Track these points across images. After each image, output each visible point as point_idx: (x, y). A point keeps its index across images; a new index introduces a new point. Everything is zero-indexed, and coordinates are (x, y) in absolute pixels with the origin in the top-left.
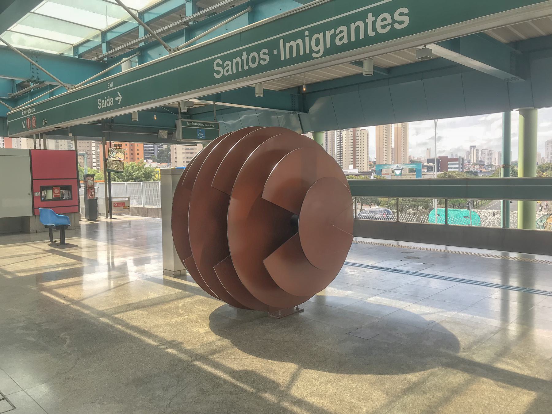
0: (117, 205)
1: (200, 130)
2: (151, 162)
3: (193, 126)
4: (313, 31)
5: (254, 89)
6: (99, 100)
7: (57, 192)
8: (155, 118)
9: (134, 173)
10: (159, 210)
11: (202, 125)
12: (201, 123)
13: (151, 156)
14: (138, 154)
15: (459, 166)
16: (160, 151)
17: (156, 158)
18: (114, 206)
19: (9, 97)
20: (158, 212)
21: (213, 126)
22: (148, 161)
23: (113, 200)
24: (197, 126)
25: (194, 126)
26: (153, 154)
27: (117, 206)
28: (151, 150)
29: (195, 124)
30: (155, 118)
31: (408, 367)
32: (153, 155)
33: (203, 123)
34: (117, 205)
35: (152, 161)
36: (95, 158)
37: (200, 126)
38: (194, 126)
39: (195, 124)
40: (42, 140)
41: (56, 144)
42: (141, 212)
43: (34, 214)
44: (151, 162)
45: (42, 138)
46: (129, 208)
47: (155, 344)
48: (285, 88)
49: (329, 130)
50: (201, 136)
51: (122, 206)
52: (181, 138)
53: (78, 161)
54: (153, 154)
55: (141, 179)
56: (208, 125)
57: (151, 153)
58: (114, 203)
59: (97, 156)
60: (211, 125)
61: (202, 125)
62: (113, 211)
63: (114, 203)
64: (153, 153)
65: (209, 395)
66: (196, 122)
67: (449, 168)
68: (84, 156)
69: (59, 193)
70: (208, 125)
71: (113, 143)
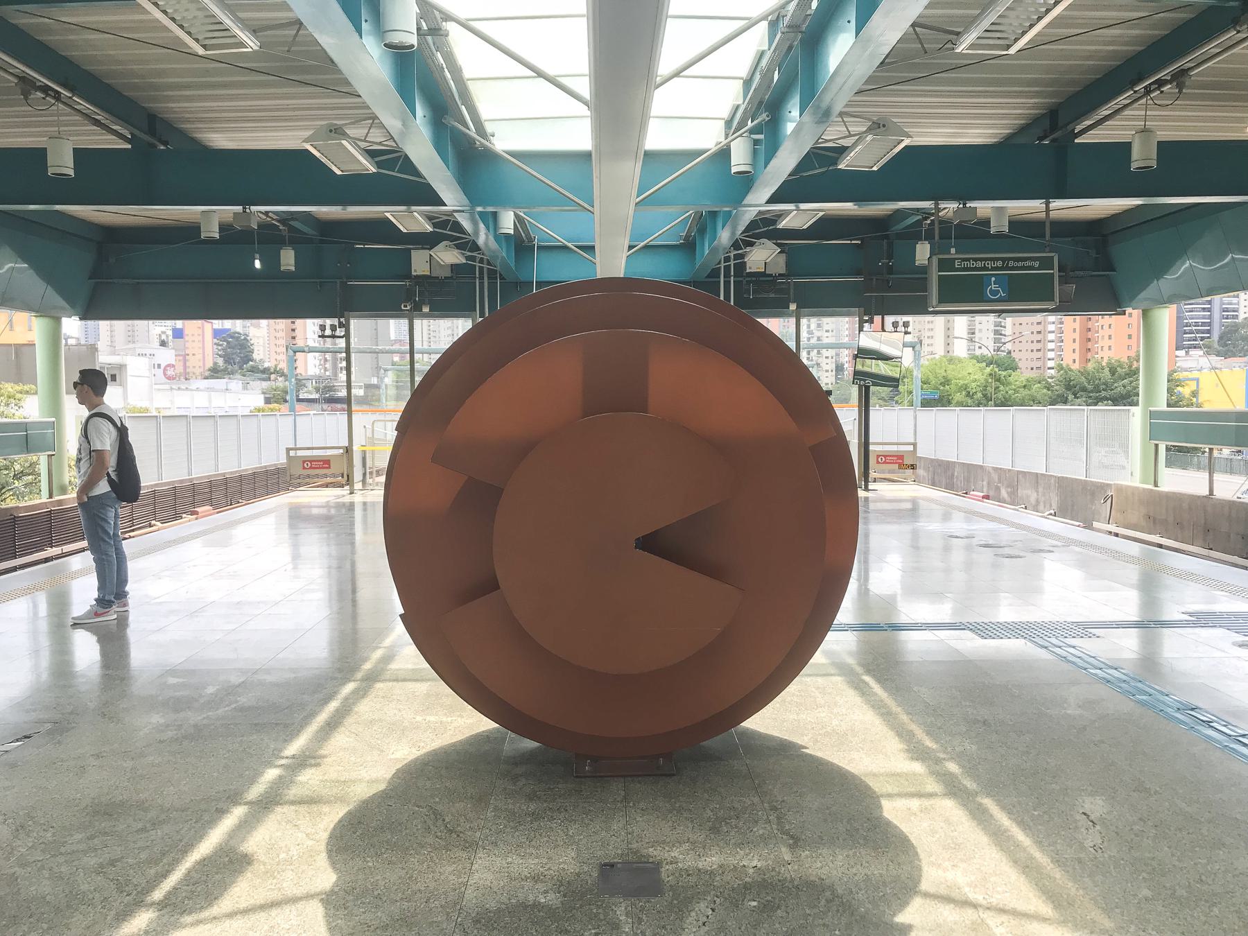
0: (884, 459)
1: (993, 279)
2: (1200, 356)
5: (1127, 147)
9: (1116, 385)
10: (1039, 478)
11: (999, 264)
12: (997, 259)
13: (1202, 339)
14: (1130, 337)
16: (1227, 327)
17: (1216, 345)
18: (878, 462)
19: (681, 241)
20: (1037, 483)
21: (1037, 264)
22: (1191, 353)
23: (871, 448)
24: (985, 269)
25: (976, 269)
26: (1209, 335)
27: (885, 463)
28: (1203, 324)
29: (979, 264)
31: (754, 923)
32: (1209, 338)
33: (1003, 260)
34: (884, 459)
35: (1201, 353)
36: (1053, 350)
37: (993, 269)
38: (976, 269)
39: (979, 264)
41: (970, 321)
42: (1006, 479)
44: (1200, 356)
46: (913, 469)
47: (988, 802)
50: (994, 293)
51: (896, 463)
52: (935, 302)
54: (1209, 335)
55: (1133, 400)
56: (1020, 264)
57: (1203, 332)
58: (878, 456)
59: (1059, 344)
60: (1028, 263)
61: (999, 264)
62: (872, 475)
63: (878, 456)
64: (1208, 332)
65: (102, 757)
66: (981, 260)
68: (913, 348)
70: (1020, 264)
71: (889, 319)
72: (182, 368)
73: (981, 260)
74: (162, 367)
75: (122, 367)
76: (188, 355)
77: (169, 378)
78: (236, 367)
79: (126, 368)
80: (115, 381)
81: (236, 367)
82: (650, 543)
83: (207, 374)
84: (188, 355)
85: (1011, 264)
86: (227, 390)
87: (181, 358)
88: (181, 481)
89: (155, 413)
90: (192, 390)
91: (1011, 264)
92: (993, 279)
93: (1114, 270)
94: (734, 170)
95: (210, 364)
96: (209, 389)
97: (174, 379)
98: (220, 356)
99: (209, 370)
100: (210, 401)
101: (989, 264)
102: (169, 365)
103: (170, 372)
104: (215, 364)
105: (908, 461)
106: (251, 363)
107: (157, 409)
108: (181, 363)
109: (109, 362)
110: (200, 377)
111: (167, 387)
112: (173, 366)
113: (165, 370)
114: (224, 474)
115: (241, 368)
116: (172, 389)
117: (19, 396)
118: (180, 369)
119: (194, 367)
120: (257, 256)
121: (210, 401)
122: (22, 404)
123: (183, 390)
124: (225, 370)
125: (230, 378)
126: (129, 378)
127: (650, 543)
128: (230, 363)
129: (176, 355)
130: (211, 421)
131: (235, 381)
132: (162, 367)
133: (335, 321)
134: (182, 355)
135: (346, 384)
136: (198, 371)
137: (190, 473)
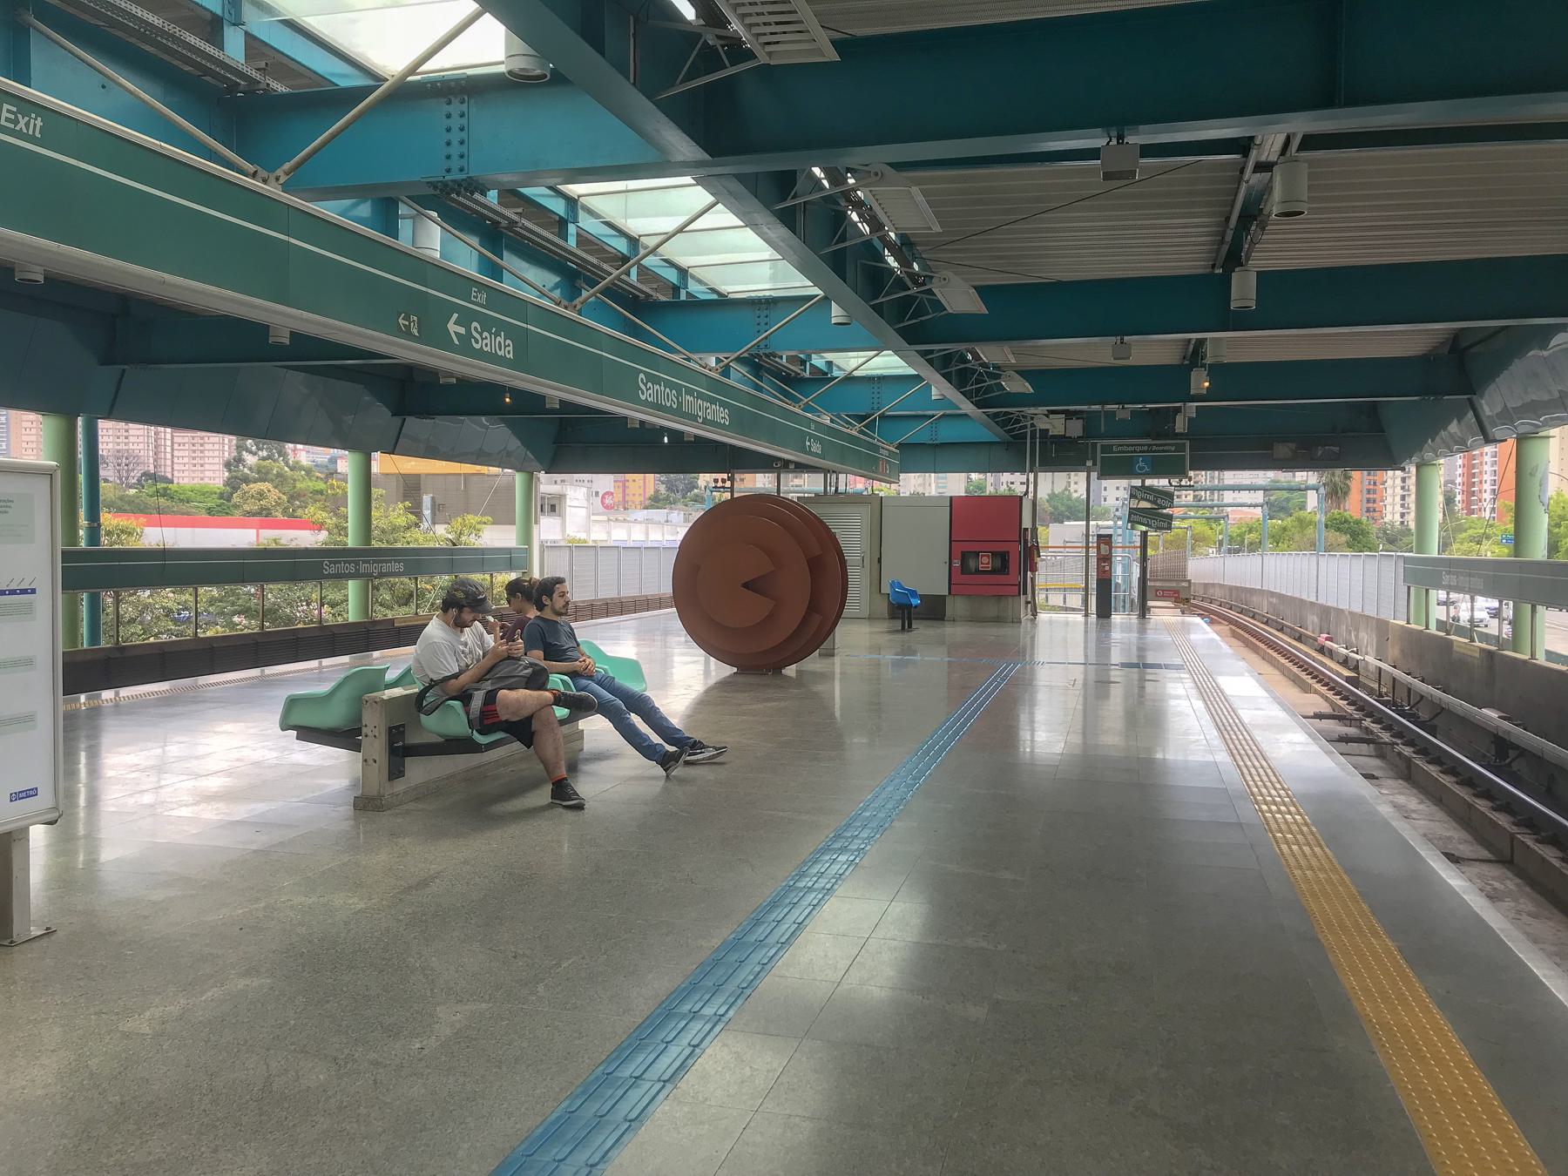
3: (1124, 452)
4: (374, 562)
6: (727, 423)
7: (985, 558)
8: (508, 400)
11: (1146, 448)
12: (1144, 445)
15: (1115, 523)
24: (1135, 452)
29: (1131, 449)
30: (508, 400)
37: (1141, 452)
39: (1131, 449)
40: (1031, 476)
43: (950, 593)
45: (1031, 471)
48: (1449, 334)
49: (290, 442)
50: (1140, 468)
53: (1149, 554)
56: (1161, 448)
67: (1121, 676)
69: (988, 563)
70: (1161, 448)
72: (621, 495)
73: (1132, 445)
74: (600, 495)
75: (562, 497)
76: (628, 481)
77: (607, 507)
78: (679, 495)
79: (565, 498)
80: (555, 511)
81: (679, 495)
82: (746, 585)
83: (647, 502)
84: (628, 481)
85: (1154, 448)
86: (667, 521)
87: (621, 484)
88: (612, 599)
89: (591, 544)
90: (628, 522)
91: (1154, 448)
92: (1141, 459)
93: (1384, 432)
94: (933, 398)
95: (650, 492)
96: (648, 521)
97: (613, 508)
98: (663, 483)
99: (650, 498)
100: (647, 534)
101: (1139, 449)
102: (607, 493)
103: (608, 501)
104: (657, 491)
105: (1183, 596)
106: (696, 491)
107: (593, 541)
108: (621, 490)
109: (548, 492)
110: (639, 507)
111: (604, 518)
112: (612, 494)
113: (603, 497)
114: (646, 596)
115: (684, 497)
116: (609, 520)
117: (478, 526)
118: (619, 497)
119: (634, 495)
120: (666, 434)
121: (647, 534)
122: (481, 533)
123: (620, 521)
124: (667, 498)
125: (671, 508)
126: (568, 509)
127: (746, 585)
128: (673, 491)
129: (615, 481)
130: (638, 552)
131: (676, 512)
132: (600, 495)
133: (725, 476)
134: (620, 481)
135: (1217, 473)
136: (638, 499)
137: (619, 593)
